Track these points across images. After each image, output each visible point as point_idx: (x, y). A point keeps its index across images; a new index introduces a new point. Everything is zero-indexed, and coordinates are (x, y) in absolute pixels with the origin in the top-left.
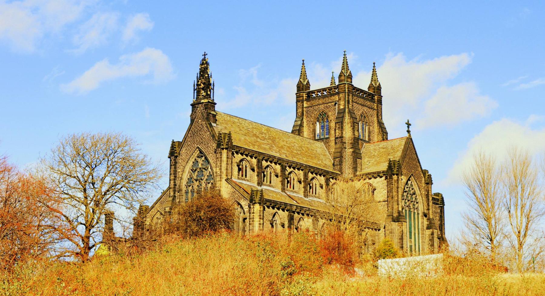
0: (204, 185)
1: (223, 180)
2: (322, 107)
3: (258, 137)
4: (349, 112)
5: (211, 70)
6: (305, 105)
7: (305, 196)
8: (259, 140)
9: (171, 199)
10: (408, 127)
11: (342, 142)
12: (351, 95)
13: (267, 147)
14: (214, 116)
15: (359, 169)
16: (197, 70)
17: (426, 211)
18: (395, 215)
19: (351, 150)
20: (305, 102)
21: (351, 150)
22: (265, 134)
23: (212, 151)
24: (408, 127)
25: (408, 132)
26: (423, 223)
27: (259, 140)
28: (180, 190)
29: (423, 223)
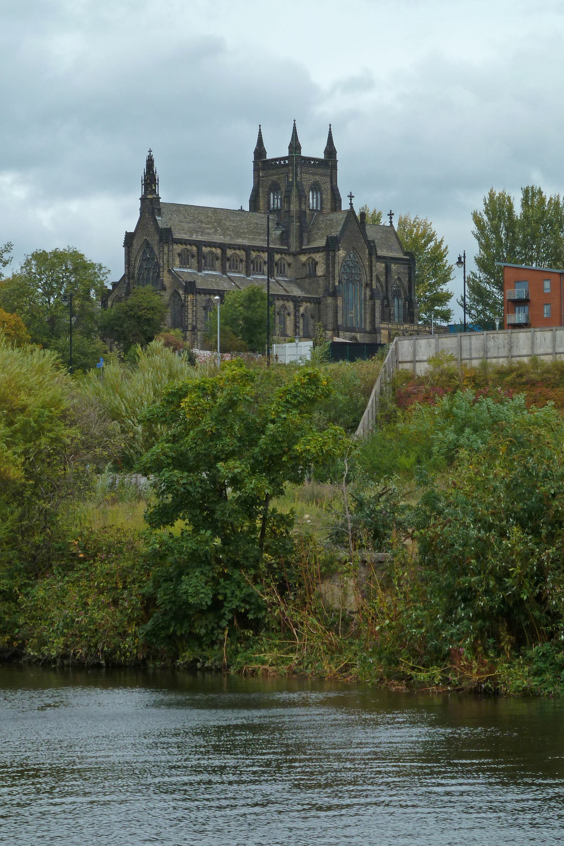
0: (151, 274)
1: (166, 271)
2: (275, 178)
3: (202, 222)
4: (297, 186)
5: (157, 166)
6: (261, 174)
7: (247, 276)
8: (204, 225)
9: (125, 286)
10: (351, 200)
11: (289, 216)
12: (299, 167)
13: (212, 231)
14: (159, 210)
15: (305, 240)
16: (143, 166)
17: (369, 282)
18: (331, 290)
19: (298, 224)
20: (261, 172)
21: (298, 224)
22: (211, 217)
23: (156, 242)
24: (351, 200)
25: (351, 204)
26: (365, 294)
27: (204, 225)
28: (133, 277)
29: (365, 294)
